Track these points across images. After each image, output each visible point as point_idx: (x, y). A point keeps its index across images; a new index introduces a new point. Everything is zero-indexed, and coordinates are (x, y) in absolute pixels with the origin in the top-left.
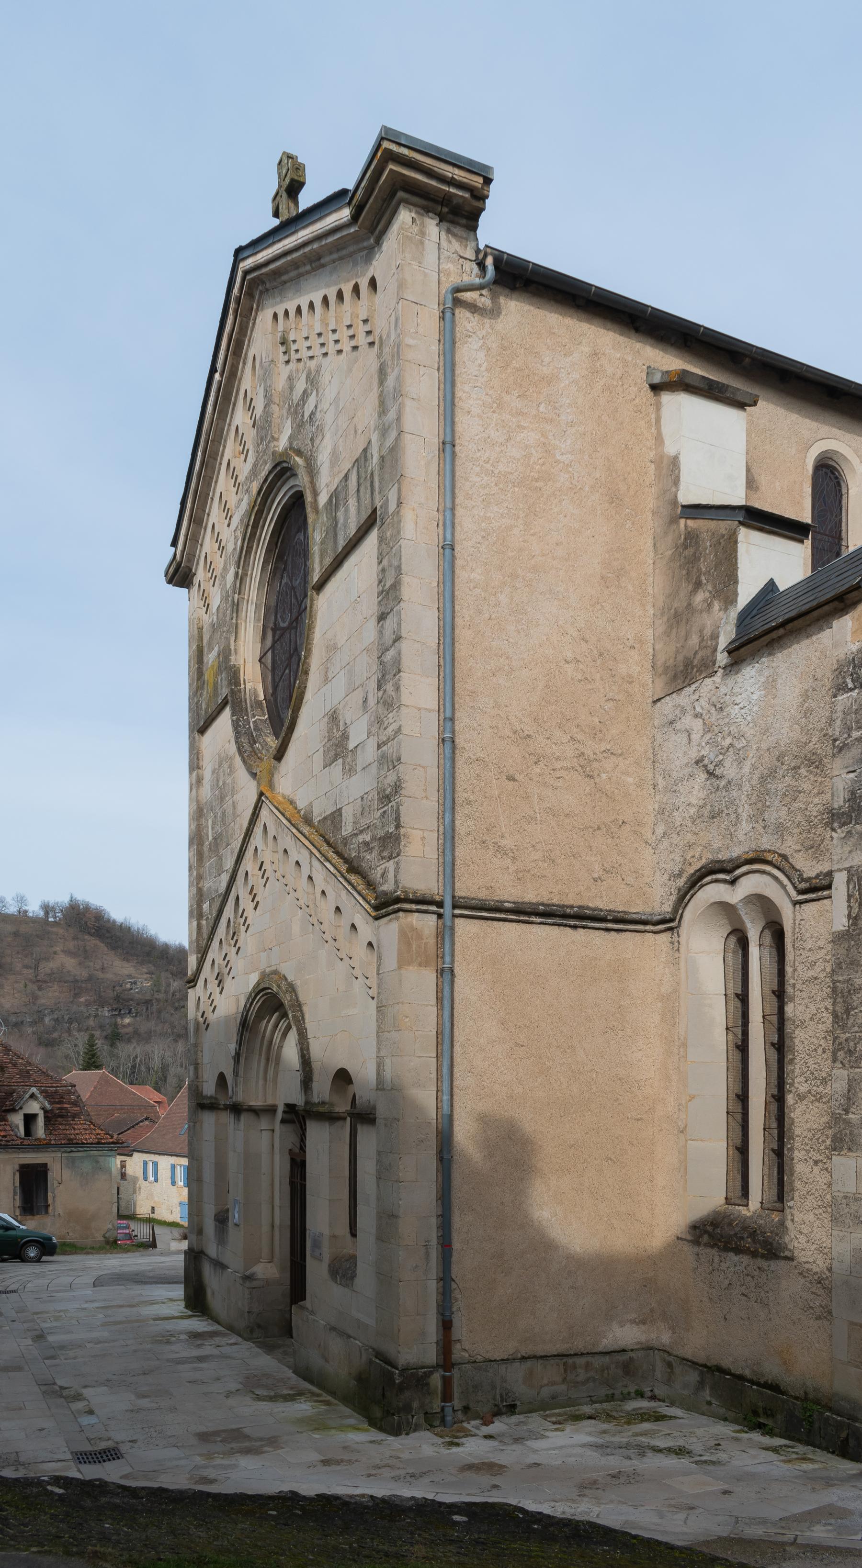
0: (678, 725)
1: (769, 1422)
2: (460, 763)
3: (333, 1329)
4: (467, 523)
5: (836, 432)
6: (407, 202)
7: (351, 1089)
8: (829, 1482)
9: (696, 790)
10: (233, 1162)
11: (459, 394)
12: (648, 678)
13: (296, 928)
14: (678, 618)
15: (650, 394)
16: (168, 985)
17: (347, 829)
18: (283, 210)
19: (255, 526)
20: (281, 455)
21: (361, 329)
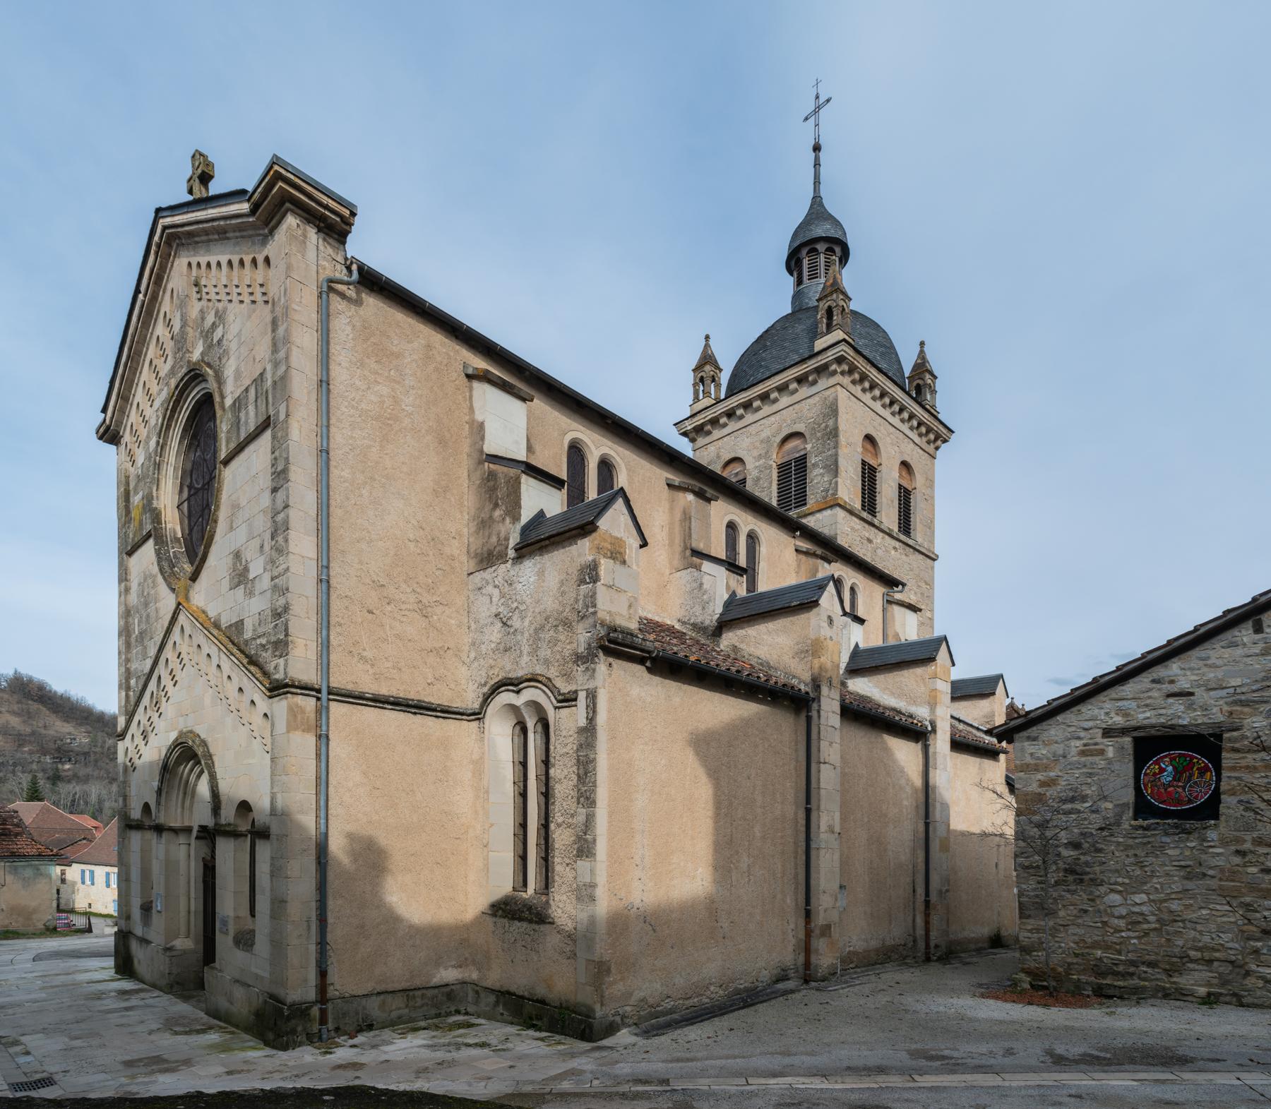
0: (484, 591)
1: (539, 1023)
2: (333, 597)
3: (237, 981)
4: (339, 438)
5: (581, 427)
6: (293, 212)
7: (251, 816)
8: (573, 1055)
9: (495, 633)
10: (156, 868)
11: (332, 350)
12: (464, 558)
13: (207, 701)
14: (484, 524)
15: (466, 380)
16: (104, 742)
17: (248, 634)
18: (196, 189)
19: (174, 410)
20: (195, 364)
21: (258, 291)
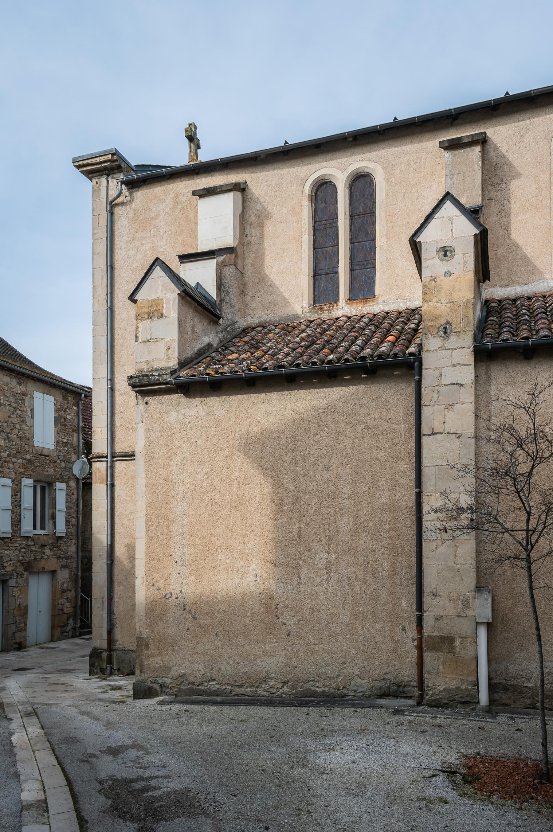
5: (324, 164)
